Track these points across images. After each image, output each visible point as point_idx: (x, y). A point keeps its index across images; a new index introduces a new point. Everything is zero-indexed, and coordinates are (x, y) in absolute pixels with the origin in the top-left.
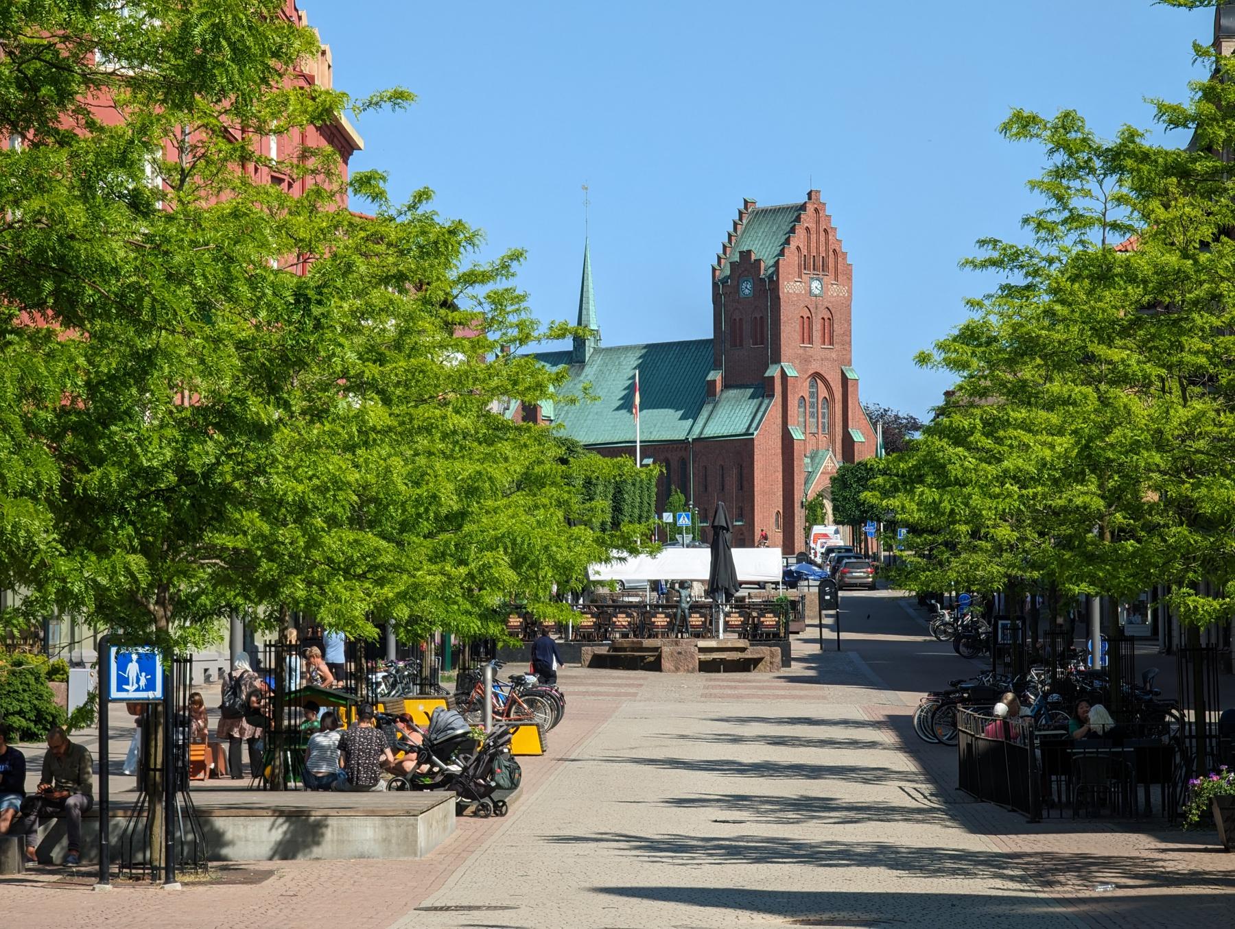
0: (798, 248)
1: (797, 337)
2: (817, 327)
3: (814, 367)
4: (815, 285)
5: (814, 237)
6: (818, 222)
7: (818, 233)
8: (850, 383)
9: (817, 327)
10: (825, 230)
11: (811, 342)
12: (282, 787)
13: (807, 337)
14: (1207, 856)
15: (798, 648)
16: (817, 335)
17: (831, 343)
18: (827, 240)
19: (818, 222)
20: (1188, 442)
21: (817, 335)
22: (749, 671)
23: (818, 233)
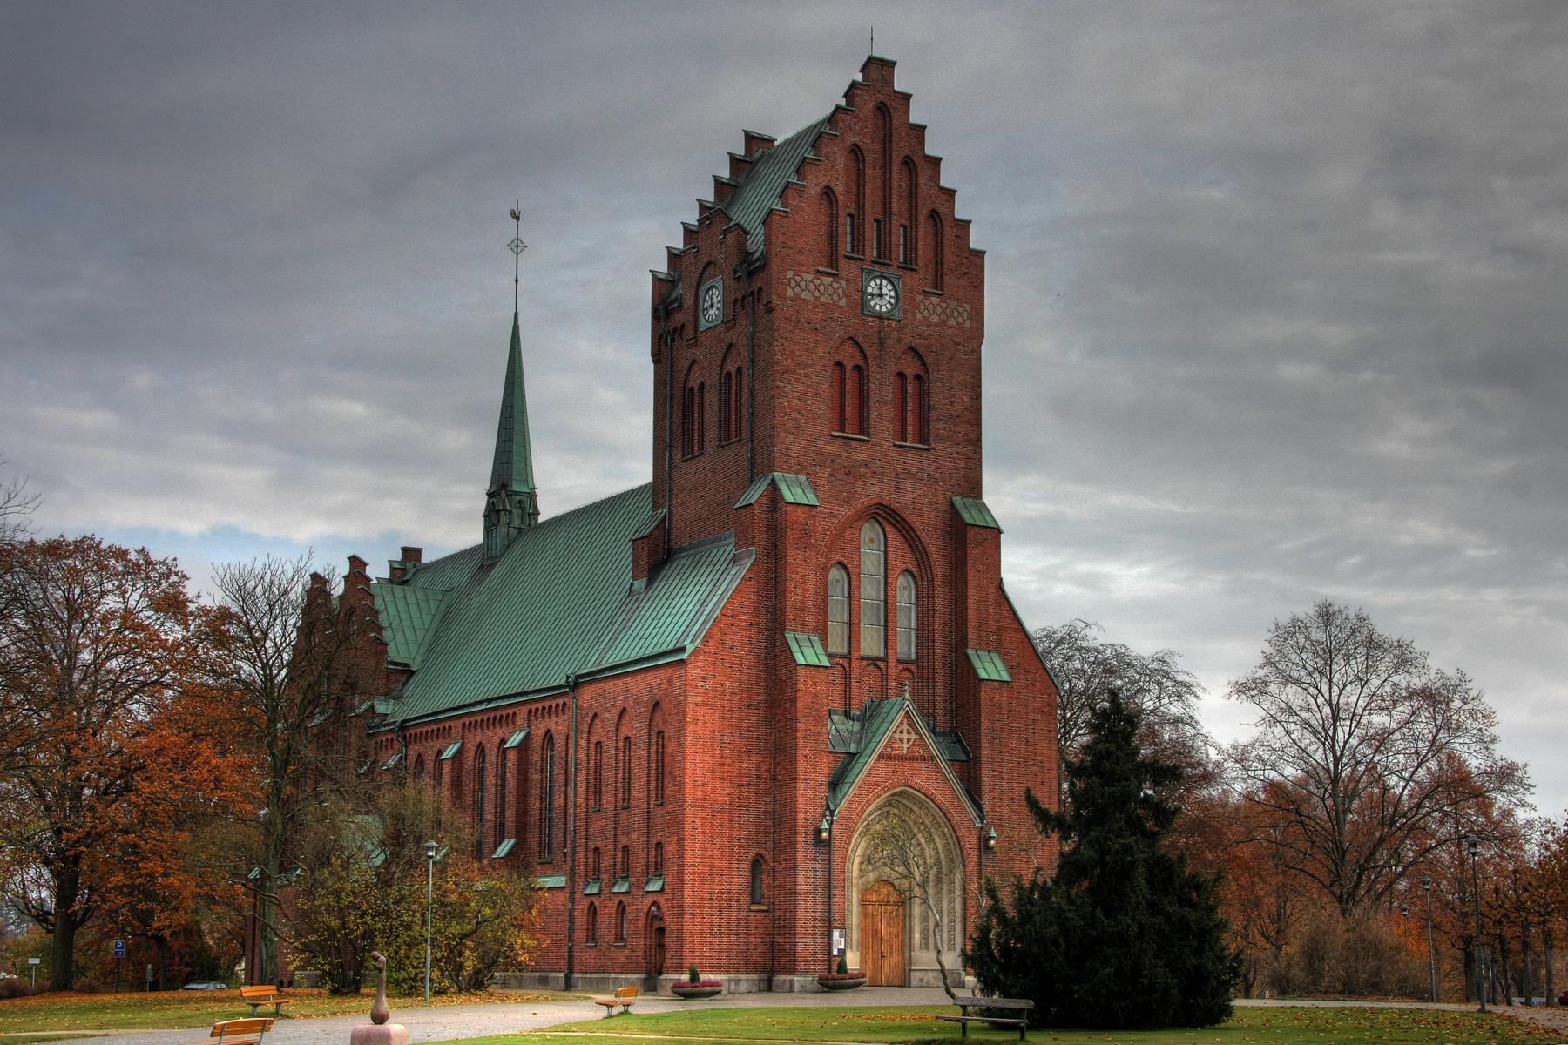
0: (828, 193)
1: (822, 409)
2: (883, 390)
3: (871, 492)
4: (883, 295)
5: (872, 174)
6: (886, 142)
7: (886, 165)
8: (971, 534)
9: (883, 390)
10: (908, 163)
11: (863, 426)
12: (705, 886)
13: (852, 415)
14: (643, 781)
15: (1230, 764)
16: (882, 417)
17: (923, 437)
18: (913, 195)
19: (886, 142)
20: (1479, 849)
21: (882, 417)
22: (175, 989)
23: (886, 165)
